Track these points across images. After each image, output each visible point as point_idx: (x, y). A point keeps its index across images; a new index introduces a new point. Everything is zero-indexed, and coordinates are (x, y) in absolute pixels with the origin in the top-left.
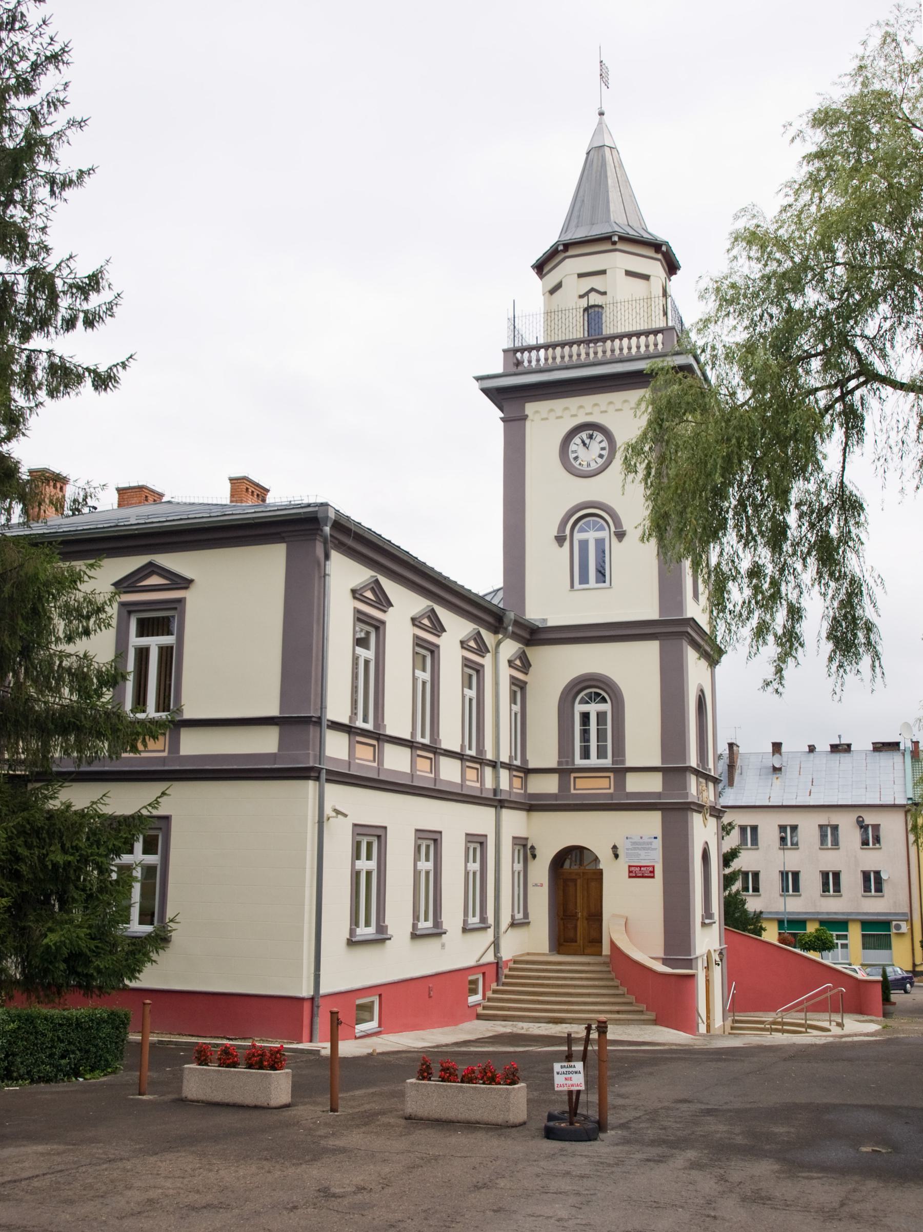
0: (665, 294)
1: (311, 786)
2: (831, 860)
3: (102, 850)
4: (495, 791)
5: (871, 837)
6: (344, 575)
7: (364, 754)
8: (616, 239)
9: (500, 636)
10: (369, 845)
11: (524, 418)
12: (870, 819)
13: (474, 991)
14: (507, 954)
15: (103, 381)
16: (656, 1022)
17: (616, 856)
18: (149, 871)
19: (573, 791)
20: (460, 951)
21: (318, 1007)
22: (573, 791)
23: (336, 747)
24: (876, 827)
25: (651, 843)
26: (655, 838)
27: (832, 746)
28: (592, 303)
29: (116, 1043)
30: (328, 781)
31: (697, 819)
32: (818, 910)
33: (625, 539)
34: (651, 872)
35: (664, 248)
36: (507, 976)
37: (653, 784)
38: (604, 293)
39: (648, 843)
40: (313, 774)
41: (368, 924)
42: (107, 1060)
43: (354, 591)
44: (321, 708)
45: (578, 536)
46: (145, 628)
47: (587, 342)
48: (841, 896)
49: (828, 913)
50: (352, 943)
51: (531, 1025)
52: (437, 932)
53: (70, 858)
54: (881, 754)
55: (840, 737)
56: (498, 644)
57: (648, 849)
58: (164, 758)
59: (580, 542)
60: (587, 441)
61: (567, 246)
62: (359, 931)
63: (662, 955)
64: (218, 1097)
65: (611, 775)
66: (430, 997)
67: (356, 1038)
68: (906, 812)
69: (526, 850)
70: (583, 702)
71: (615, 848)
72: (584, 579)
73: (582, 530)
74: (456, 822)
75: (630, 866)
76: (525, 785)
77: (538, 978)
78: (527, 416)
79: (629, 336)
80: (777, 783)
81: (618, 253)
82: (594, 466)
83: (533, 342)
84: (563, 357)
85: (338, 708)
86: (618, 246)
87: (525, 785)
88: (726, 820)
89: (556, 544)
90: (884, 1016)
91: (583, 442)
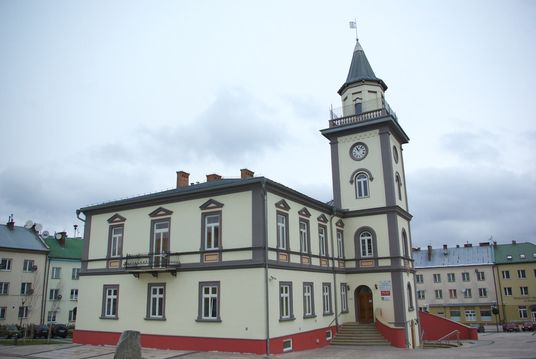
0: (383, 97)
4: (333, 268)
5: (481, 276)
6: (272, 199)
7: (283, 258)
10: (286, 288)
12: (480, 270)
14: (340, 323)
17: (377, 288)
18: (161, 299)
20: (322, 322)
23: (272, 256)
24: (483, 273)
30: (269, 268)
31: (404, 274)
37: (387, 263)
38: (361, 99)
40: (264, 266)
41: (327, 310)
43: (276, 205)
45: (358, 181)
46: (159, 227)
47: (356, 116)
50: (281, 321)
52: (313, 316)
56: (332, 218)
62: (307, 314)
63: (394, 321)
65: (218, 253)
69: (345, 287)
71: (376, 285)
72: (360, 195)
73: (359, 178)
74: (318, 279)
76: (344, 265)
80: (446, 259)
82: (361, 157)
83: (339, 117)
85: (272, 242)
88: (417, 273)
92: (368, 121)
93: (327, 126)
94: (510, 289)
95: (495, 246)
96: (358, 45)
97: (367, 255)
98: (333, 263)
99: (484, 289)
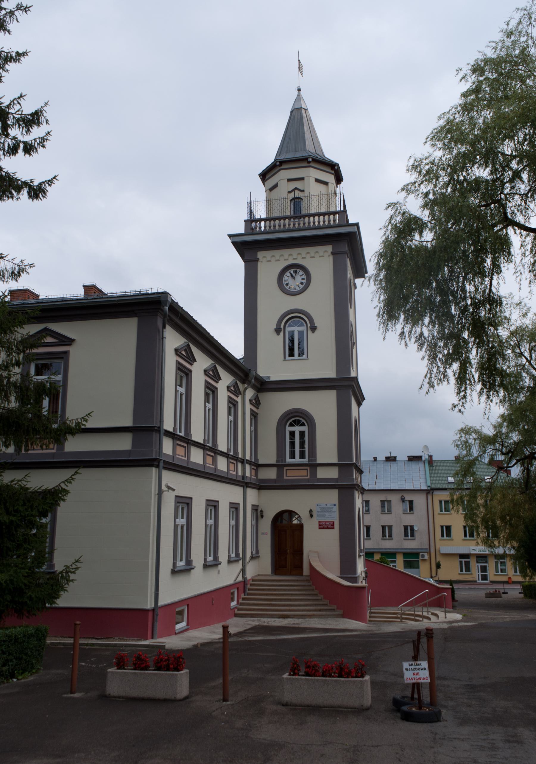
1: (154, 471)
2: (387, 520)
3: (35, 512)
4: (244, 477)
6: (173, 340)
8: (311, 160)
9: (246, 386)
11: (257, 260)
13: (233, 600)
14: (249, 575)
15: (37, 192)
16: (343, 616)
17: (311, 516)
19: (285, 478)
20: (227, 576)
21: (157, 615)
22: (285, 478)
25: (332, 508)
26: (335, 505)
27: (386, 458)
28: (297, 196)
29: (39, 650)
30: (165, 468)
32: (380, 547)
33: (316, 332)
34: (332, 525)
35: (336, 167)
36: (249, 589)
37: (333, 473)
38: (303, 191)
39: (330, 508)
40: (156, 463)
42: (32, 664)
44: (160, 422)
45: (288, 329)
47: (295, 218)
48: (392, 539)
49: (385, 549)
51: (269, 619)
53: (14, 518)
54: (413, 462)
55: (390, 453)
56: (245, 389)
57: (331, 512)
58: (54, 453)
59: (289, 332)
60: (294, 275)
61: (282, 163)
64: (135, 693)
65: (308, 468)
66: (213, 604)
67: (176, 634)
68: (427, 494)
70: (291, 425)
71: (311, 511)
72: (292, 354)
73: (290, 326)
75: (319, 522)
76: (256, 474)
77: (269, 590)
78: (259, 259)
79: (319, 215)
81: (311, 169)
82: (297, 289)
84: (280, 226)
85: (168, 425)
86: (311, 164)
87: (256, 474)
89: (275, 334)
90: (453, 608)
91: (291, 275)
92: (315, 228)
93: (241, 229)
94: (448, 528)
95: (431, 461)
96: (299, 98)
97: (297, 460)
98: (244, 470)
99: (412, 527)
